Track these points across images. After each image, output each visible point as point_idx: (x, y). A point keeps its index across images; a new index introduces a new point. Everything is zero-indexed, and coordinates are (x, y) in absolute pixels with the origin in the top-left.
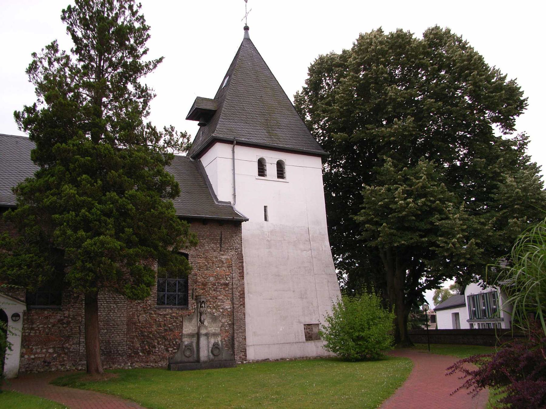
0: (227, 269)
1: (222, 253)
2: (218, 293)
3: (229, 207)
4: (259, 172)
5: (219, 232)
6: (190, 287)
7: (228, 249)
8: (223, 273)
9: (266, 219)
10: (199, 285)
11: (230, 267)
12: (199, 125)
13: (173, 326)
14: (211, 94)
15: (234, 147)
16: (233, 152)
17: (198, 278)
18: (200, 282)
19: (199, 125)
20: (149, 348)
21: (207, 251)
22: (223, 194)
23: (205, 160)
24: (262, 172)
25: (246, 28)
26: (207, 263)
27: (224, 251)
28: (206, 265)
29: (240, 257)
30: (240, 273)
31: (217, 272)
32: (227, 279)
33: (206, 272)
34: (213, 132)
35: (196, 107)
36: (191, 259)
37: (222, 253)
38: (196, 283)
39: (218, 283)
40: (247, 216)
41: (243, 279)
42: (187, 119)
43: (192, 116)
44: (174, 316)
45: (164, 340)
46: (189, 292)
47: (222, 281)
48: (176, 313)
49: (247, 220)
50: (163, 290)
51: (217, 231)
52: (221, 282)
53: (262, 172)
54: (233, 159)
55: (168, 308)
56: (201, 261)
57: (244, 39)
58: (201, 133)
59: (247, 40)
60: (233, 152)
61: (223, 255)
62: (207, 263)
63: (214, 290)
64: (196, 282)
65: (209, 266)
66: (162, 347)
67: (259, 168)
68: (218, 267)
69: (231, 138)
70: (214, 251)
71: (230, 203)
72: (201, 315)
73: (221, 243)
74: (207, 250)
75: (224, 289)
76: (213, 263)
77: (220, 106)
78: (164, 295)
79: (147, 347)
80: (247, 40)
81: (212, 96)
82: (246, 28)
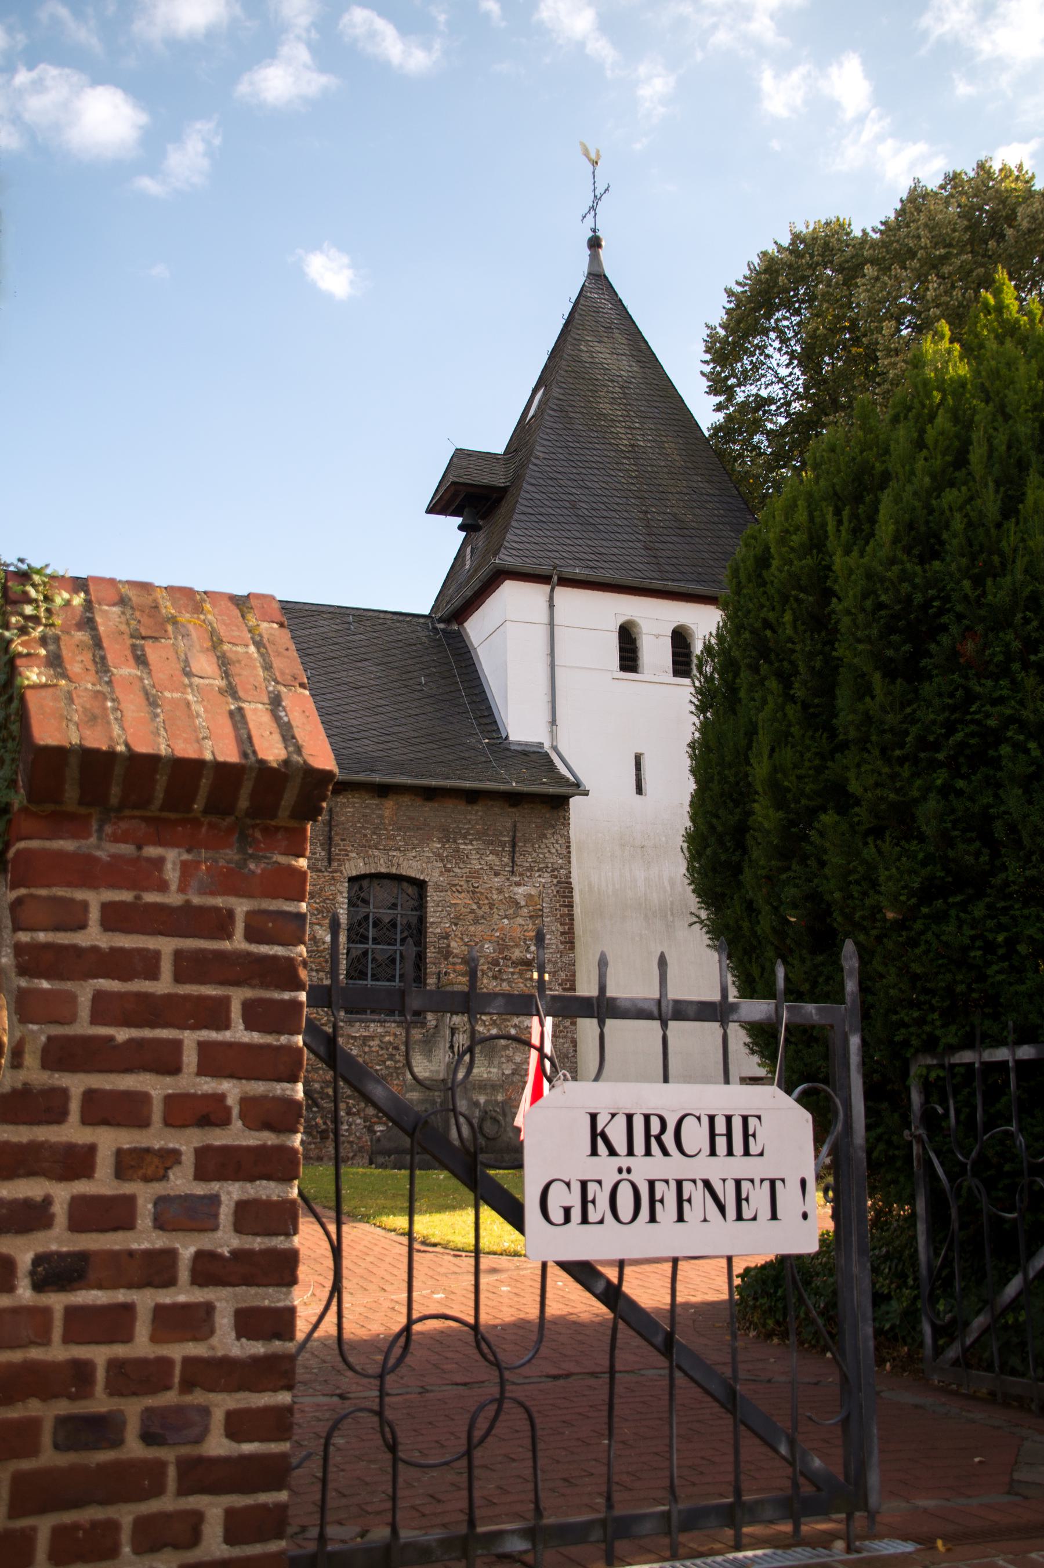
0: (530, 922)
1: (517, 879)
2: (505, 984)
3: (537, 759)
4: (622, 658)
5: (509, 825)
6: (431, 969)
7: (531, 869)
8: (518, 933)
9: (639, 790)
10: (454, 964)
11: (537, 916)
12: (461, 528)
13: (387, 1067)
14: (495, 440)
15: (552, 590)
16: (551, 606)
17: (453, 944)
18: (456, 956)
19: (461, 528)
20: (325, 1123)
21: (475, 874)
22: (522, 723)
23: (477, 628)
24: (629, 657)
25: (595, 243)
26: (475, 907)
27: (521, 875)
28: (472, 911)
29: (565, 889)
30: (563, 933)
31: (502, 929)
32: (527, 950)
33: (472, 929)
34: (496, 553)
35: (451, 479)
36: (433, 896)
37: (517, 879)
38: (446, 959)
39: (504, 958)
40: (587, 783)
41: (572, 948)
42: (430, 510)
43: (439, 506)
44: (390, 1043)
45: (362, 1105)
46: (429, 981)
47: (517, 954)
48: (395, 1035)
49: (586, 793)
50: (364, 939)
51: (504, 819)
52: (514, 958)
53: (629, 657)
54: (551, 624)
55: (374, 1021)
56: (462, 900)
57: (590, 274)
58: (469, 550)
59: (597, 278)
60: (551, 606)
61: (518, 884)
62: (475, 907)
63: (495, 978)
64: (446, 953)
65: (480, 913)
66: (359, 1121)
67: (674, 654)
68: (506, 917)
69: (545, 569)
70: (496, 874)
71: (541, 745)
72: (453, 1035)
73: (514, 852)
74: (476, 871)
75: (521, 974)
76: (491, 906)
77: (517, 479)
78: (365, 953)
79: (319, 1120)
80: (597, 278)
81: (499, 447)
82: (595, 243)
